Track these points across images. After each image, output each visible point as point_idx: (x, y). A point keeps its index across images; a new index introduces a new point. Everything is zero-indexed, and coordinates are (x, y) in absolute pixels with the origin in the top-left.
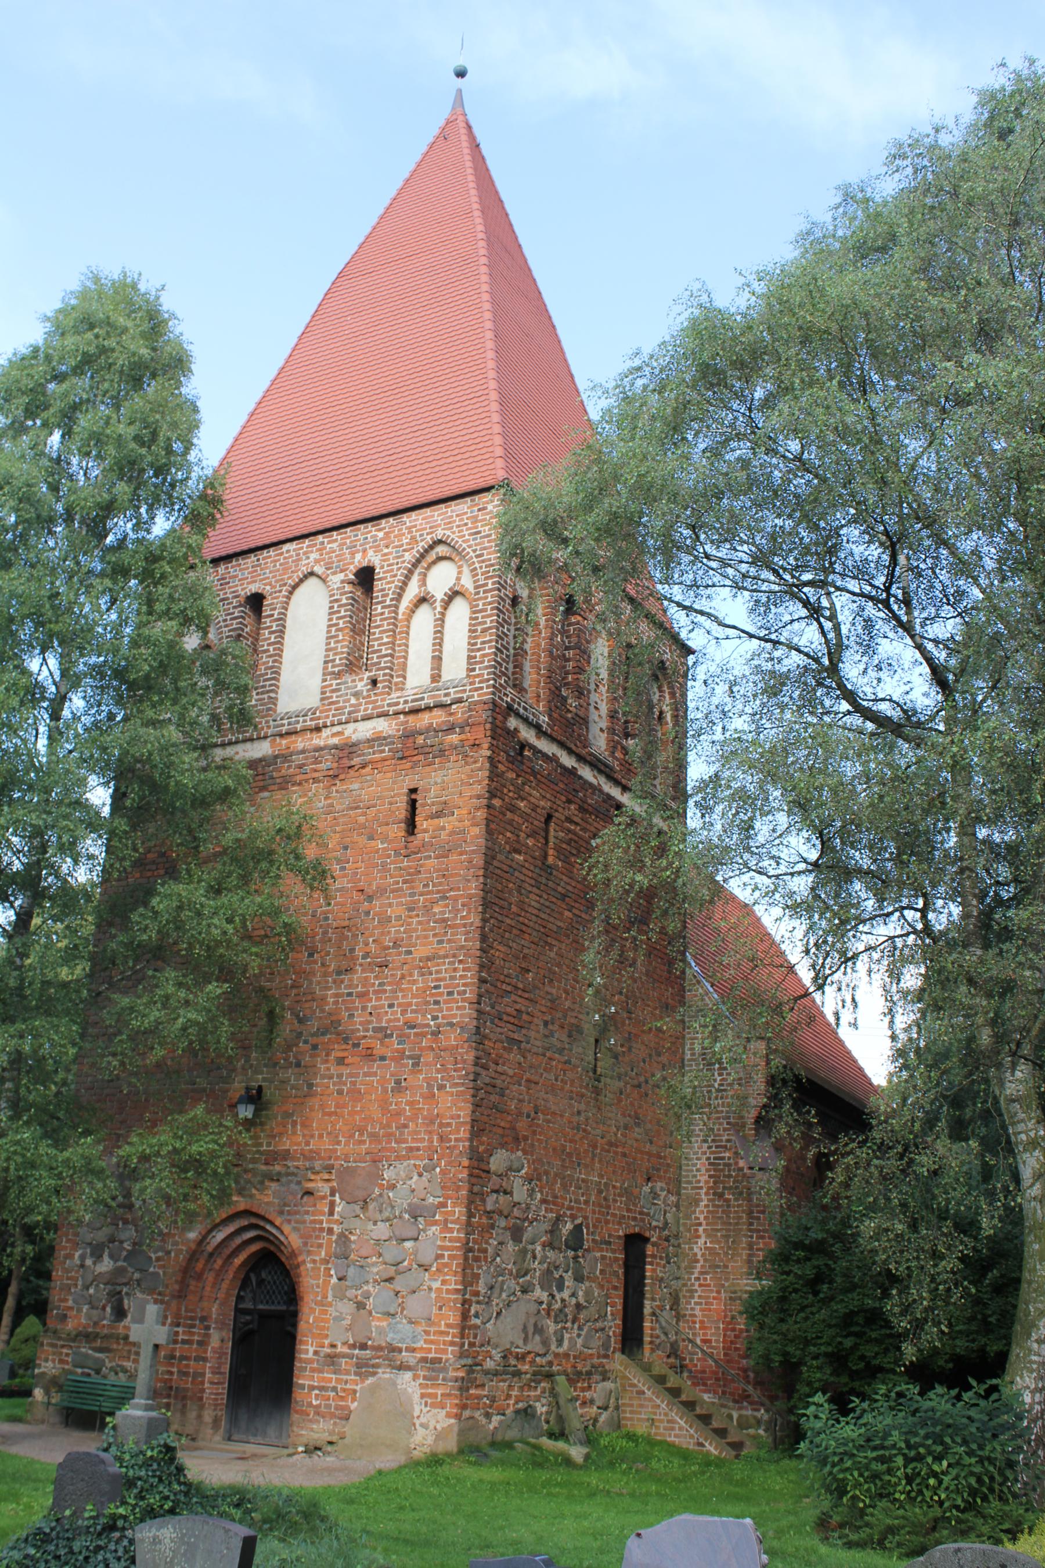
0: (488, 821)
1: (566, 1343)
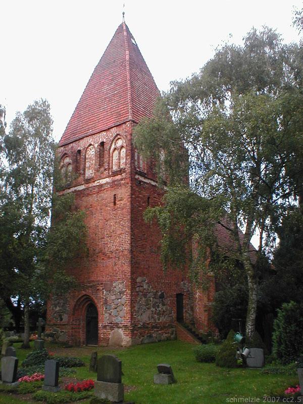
0: (131, 201)
1: (161, 320)
